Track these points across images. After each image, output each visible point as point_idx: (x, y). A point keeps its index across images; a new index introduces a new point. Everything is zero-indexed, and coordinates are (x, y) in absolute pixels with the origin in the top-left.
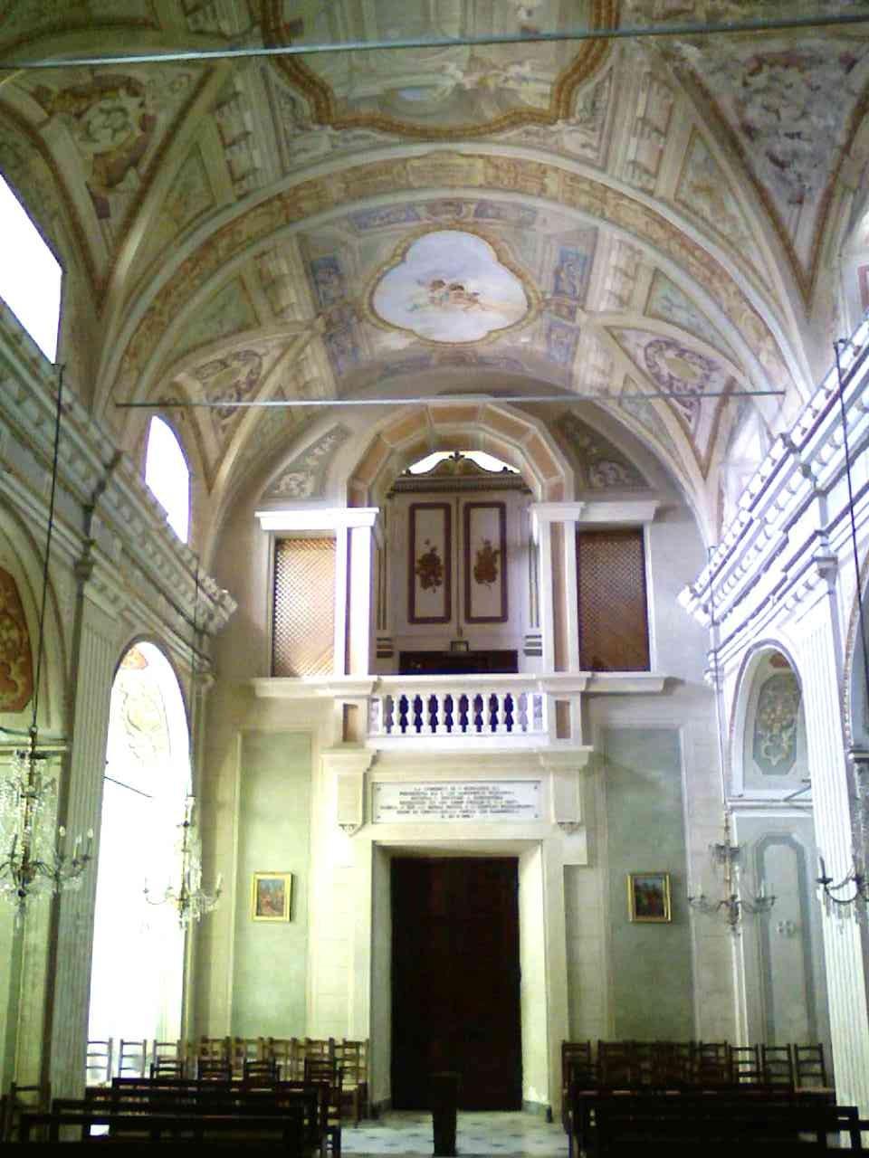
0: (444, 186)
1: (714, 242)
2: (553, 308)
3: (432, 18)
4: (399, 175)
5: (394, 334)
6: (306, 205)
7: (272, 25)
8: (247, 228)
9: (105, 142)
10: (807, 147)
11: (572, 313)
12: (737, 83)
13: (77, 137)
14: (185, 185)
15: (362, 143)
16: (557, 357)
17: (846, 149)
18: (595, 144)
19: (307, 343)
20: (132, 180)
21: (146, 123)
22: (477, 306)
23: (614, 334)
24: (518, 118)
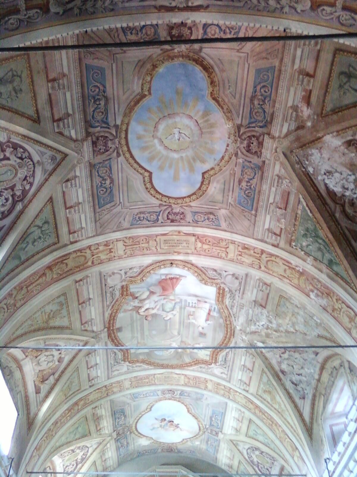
0: (168, 384)
1: (273, 411)
2: (209, 431)
3: (168, 327)
4: (152, 380)
5: (144, 439)
6: (115, 390)
7: (112, 328)
8: (91, 398)
9: (44, 366)
10: (304, 379)
11: (217, 434)
12: (278, 356)
13: (34, 364)
14: (71, 382)
15: (138, 369)
16: (211, 451)
17: (319, 380)
18: (226, 373)
19: (108, 442)
20: (52, 380)
21: (60, 360)
22: (178, 429)
23: (234, 444)
24: (197, 362)
